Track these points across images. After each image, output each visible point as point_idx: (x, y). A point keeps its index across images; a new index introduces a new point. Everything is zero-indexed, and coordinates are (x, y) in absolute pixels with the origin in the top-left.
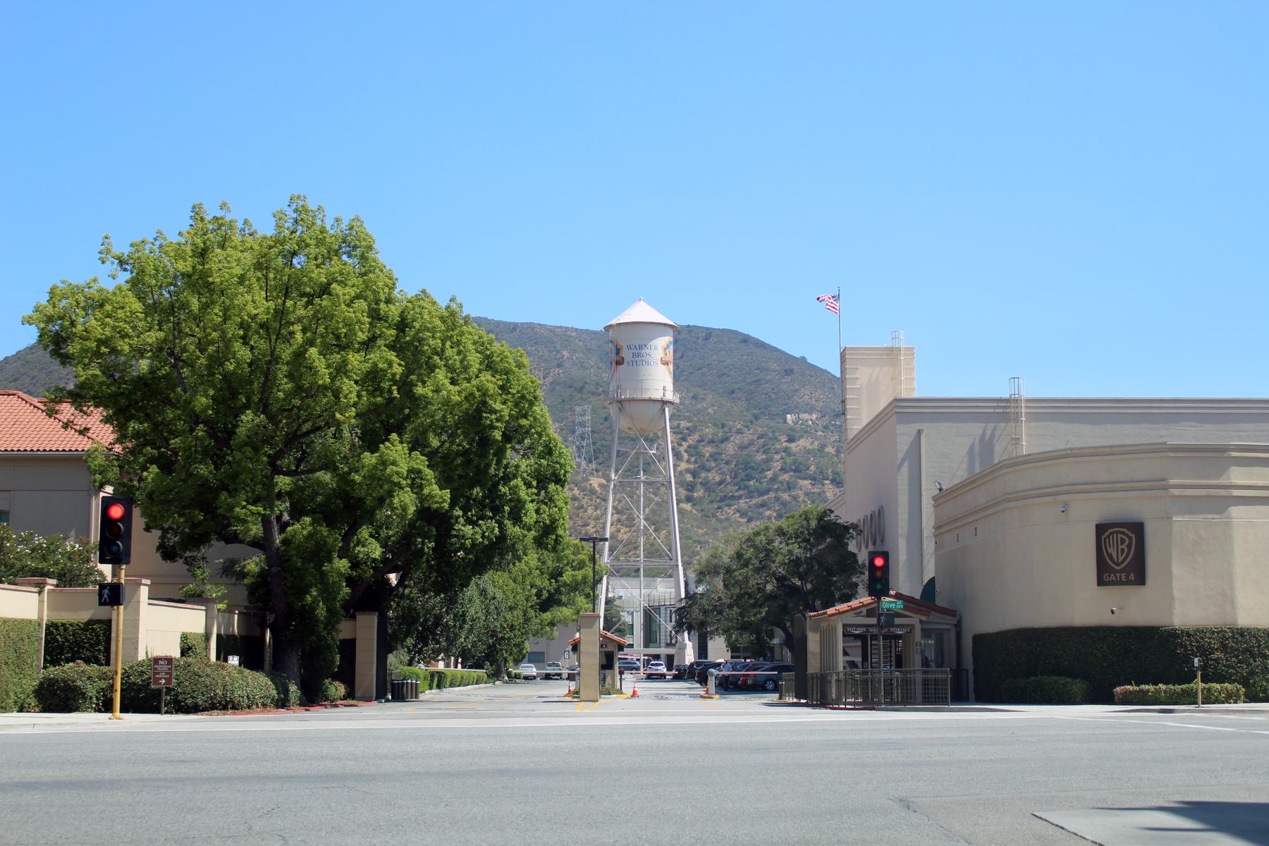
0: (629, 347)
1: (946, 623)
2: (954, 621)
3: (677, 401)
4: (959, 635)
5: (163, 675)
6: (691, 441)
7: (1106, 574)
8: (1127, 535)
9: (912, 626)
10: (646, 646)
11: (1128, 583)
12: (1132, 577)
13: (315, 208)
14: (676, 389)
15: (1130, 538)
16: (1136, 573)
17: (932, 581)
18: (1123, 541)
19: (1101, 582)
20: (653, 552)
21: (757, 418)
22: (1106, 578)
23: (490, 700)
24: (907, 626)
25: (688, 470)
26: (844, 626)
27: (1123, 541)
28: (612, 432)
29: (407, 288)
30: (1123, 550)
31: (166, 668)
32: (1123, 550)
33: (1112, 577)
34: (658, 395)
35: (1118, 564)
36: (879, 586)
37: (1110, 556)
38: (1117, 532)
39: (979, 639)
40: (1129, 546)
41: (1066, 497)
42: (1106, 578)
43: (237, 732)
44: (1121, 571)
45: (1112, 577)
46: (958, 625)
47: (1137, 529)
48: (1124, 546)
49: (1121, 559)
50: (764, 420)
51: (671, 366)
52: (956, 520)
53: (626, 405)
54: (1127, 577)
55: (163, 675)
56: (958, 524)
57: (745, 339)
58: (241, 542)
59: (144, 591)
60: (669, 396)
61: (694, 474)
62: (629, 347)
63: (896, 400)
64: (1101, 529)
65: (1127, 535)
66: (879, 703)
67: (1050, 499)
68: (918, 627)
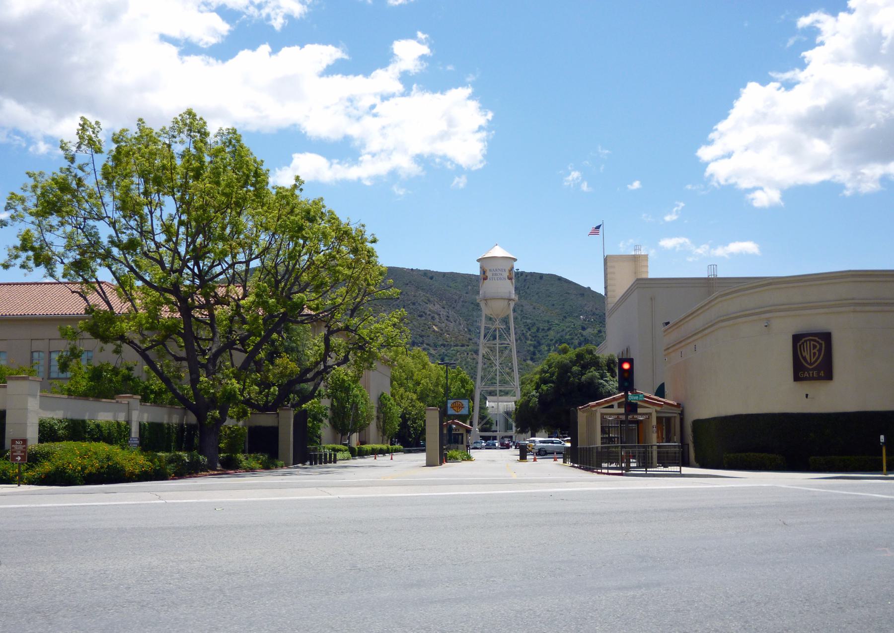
0: (490, 270)
4: (682, 421)
6: (534, 330)
7: (800, 372)
8: (818, 342)
9: (650, 414)
11: (819, 378)
12: (822, 374)
13: (293, 182)
16: (825, 371)
18: (815, 347)
19: (797, 378)
20: (503, 382)
21: (565, 317)
22: (800, 374)
23: (33, 493)
24: (646, 414)
25: (530, 345)
27: (815, 347)
28: (480, 316)
29: (344, 220)
30: (815, 354)
31: (21, 447)
32: (815, 354)
33: (806, 374)
35: (811, 364)
36: (626, 384)
37: (804, 358)
38: (810, 340)
39: (697, 424)
40: (820, 351)
41: (768, 315)
42: (800, 374)
44: (813, 369)
45: (806, 374)
46: (682, 414)
47: (826, 337)
48: (815, 351)
49: (813, 360)
50: (569, 319)
52: (681, 342)
53: (489, 302)
54: (818, 373)
55: (19, 453)
56: (683, 344)
57: (560, 279)
58: (174, 356)
60: (513, 296)
61: (535, 347)
62: (490, 270)
63: (638, 280)
64: (797, 339)
65: (818, 342)
67: (755, 317)
68: (654, 416)
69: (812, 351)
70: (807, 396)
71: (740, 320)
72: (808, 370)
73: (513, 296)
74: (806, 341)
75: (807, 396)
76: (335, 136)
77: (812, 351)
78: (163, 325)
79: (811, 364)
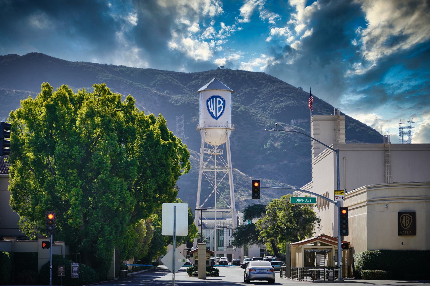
7: (401, 231)
9: (332, 249)
16: (412, 231)
18: (408, 219)
19: (400, 234)
24: (330, 249)
27: (408, 219)
30: (407, 222)
32: (407, 222)
33: (404, 232)
35: (406, 227)
37: (403, 224)
38: (405, 215)
40: (410, 221)
45: (404, 232)
48: (408, 221)
49: (407, 225)
64: (400, 214)
69: (218, 106)
70: (402, 243)
71: (375, 203)
72: (404, 230)
73: (230, 126)
74: (404, 216)
75: (402, 243)
76: (377, 25)
77: (218, 106)
78: (139, 149)
79: (406, 227)
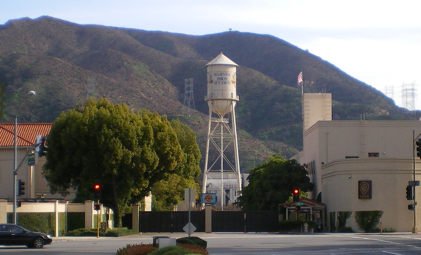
1: (322, 207)
2: (324, 207)
3: (238, 100)
4: (326, 211)
5: (104, 227)
9: (310, 209)
10: (220, 179)
11: (366, 198)
14: (237, 94)
15: (368, 185)
17: (321, 192)
26: (289, 209)
34: (230, 97)
35: (364, 193)
38: (364, 183)
43: (318, 235)
44: (365, 194)
46: (326, 208)
47: (370, 182)
49: (365, 191)
51: (236, 84)
55: (104, 227)
59: (102, 206)
66: (325, 231)
